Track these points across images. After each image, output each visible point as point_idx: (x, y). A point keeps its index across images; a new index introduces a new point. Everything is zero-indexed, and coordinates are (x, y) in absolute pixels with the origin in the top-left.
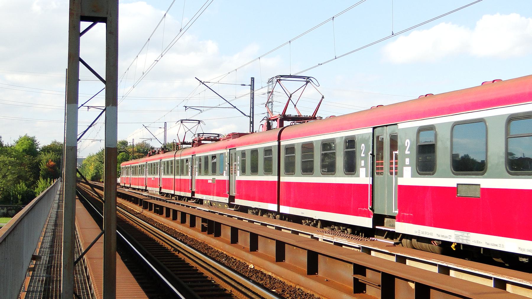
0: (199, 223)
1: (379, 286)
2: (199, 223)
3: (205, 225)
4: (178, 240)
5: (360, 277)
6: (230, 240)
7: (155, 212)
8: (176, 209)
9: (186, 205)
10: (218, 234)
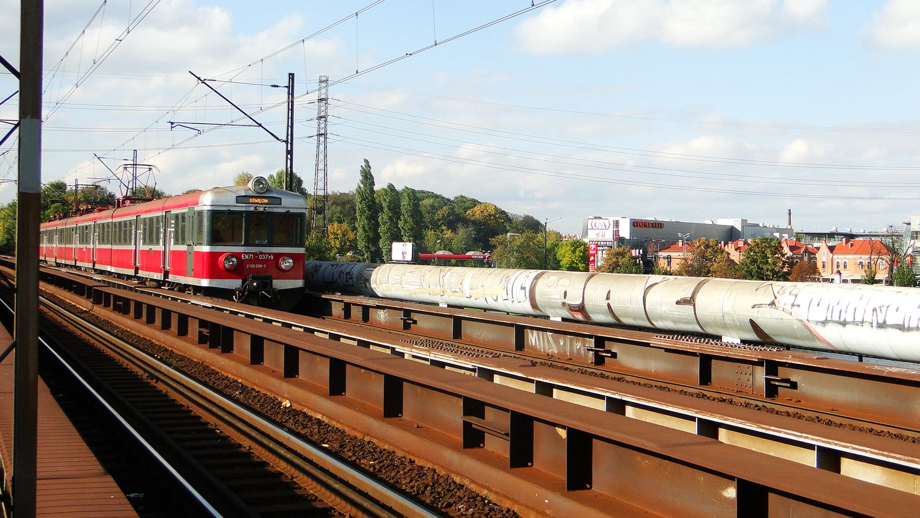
0: (194, 328)
1: (507, 435)
2: (194, 328)
3: (206, 332)
4: (156, 358)
5: (474, 420)
6: (327, 387)
7: (114, 309)
8: (153, 303)
9: (171, 297)
10: (227, 348)
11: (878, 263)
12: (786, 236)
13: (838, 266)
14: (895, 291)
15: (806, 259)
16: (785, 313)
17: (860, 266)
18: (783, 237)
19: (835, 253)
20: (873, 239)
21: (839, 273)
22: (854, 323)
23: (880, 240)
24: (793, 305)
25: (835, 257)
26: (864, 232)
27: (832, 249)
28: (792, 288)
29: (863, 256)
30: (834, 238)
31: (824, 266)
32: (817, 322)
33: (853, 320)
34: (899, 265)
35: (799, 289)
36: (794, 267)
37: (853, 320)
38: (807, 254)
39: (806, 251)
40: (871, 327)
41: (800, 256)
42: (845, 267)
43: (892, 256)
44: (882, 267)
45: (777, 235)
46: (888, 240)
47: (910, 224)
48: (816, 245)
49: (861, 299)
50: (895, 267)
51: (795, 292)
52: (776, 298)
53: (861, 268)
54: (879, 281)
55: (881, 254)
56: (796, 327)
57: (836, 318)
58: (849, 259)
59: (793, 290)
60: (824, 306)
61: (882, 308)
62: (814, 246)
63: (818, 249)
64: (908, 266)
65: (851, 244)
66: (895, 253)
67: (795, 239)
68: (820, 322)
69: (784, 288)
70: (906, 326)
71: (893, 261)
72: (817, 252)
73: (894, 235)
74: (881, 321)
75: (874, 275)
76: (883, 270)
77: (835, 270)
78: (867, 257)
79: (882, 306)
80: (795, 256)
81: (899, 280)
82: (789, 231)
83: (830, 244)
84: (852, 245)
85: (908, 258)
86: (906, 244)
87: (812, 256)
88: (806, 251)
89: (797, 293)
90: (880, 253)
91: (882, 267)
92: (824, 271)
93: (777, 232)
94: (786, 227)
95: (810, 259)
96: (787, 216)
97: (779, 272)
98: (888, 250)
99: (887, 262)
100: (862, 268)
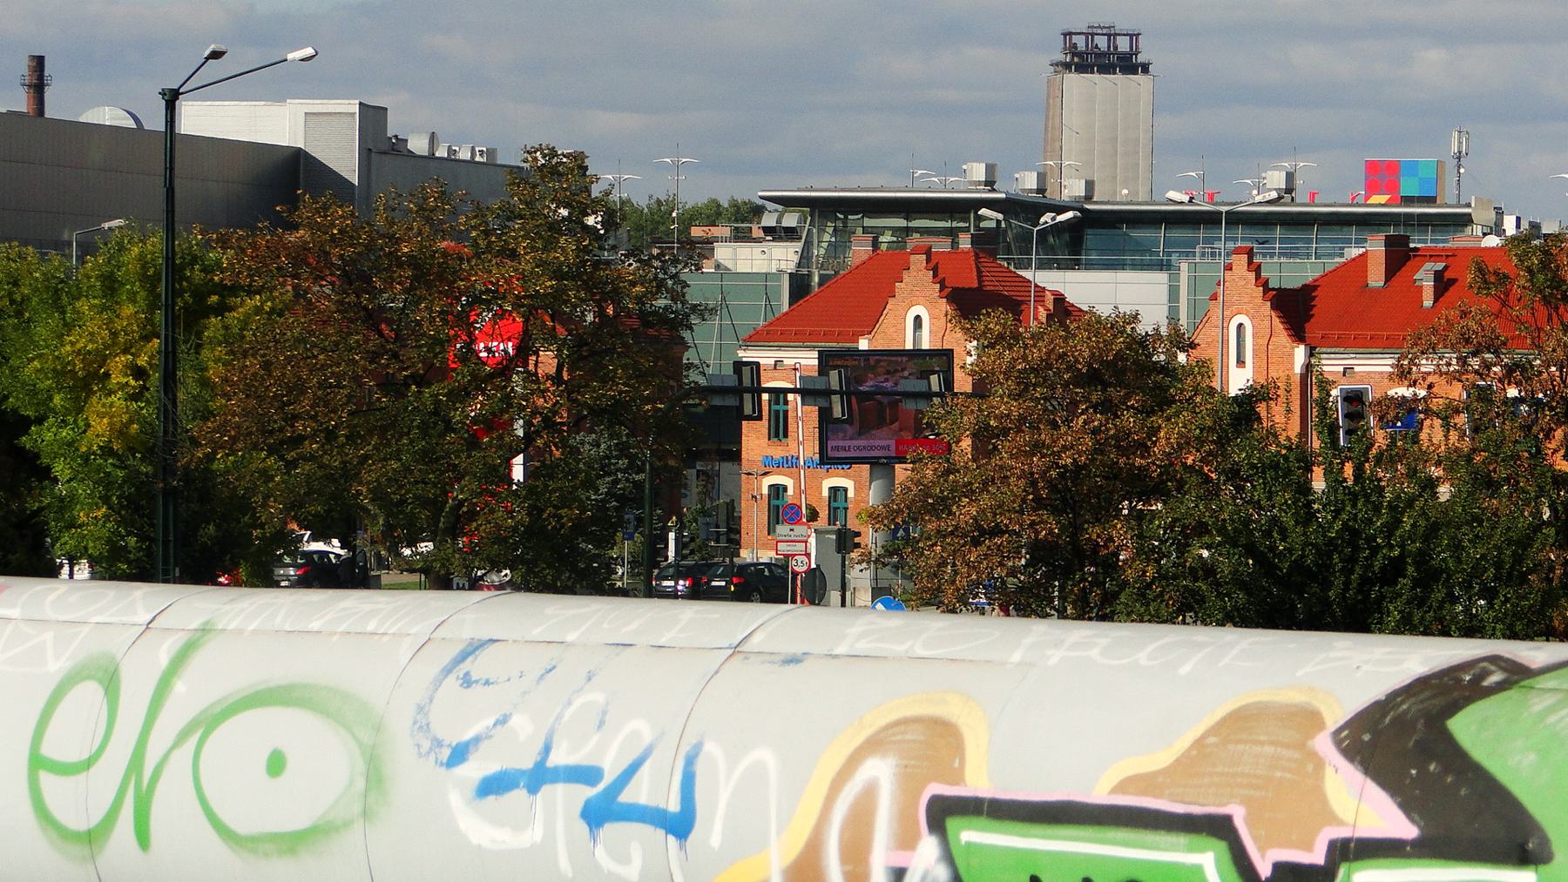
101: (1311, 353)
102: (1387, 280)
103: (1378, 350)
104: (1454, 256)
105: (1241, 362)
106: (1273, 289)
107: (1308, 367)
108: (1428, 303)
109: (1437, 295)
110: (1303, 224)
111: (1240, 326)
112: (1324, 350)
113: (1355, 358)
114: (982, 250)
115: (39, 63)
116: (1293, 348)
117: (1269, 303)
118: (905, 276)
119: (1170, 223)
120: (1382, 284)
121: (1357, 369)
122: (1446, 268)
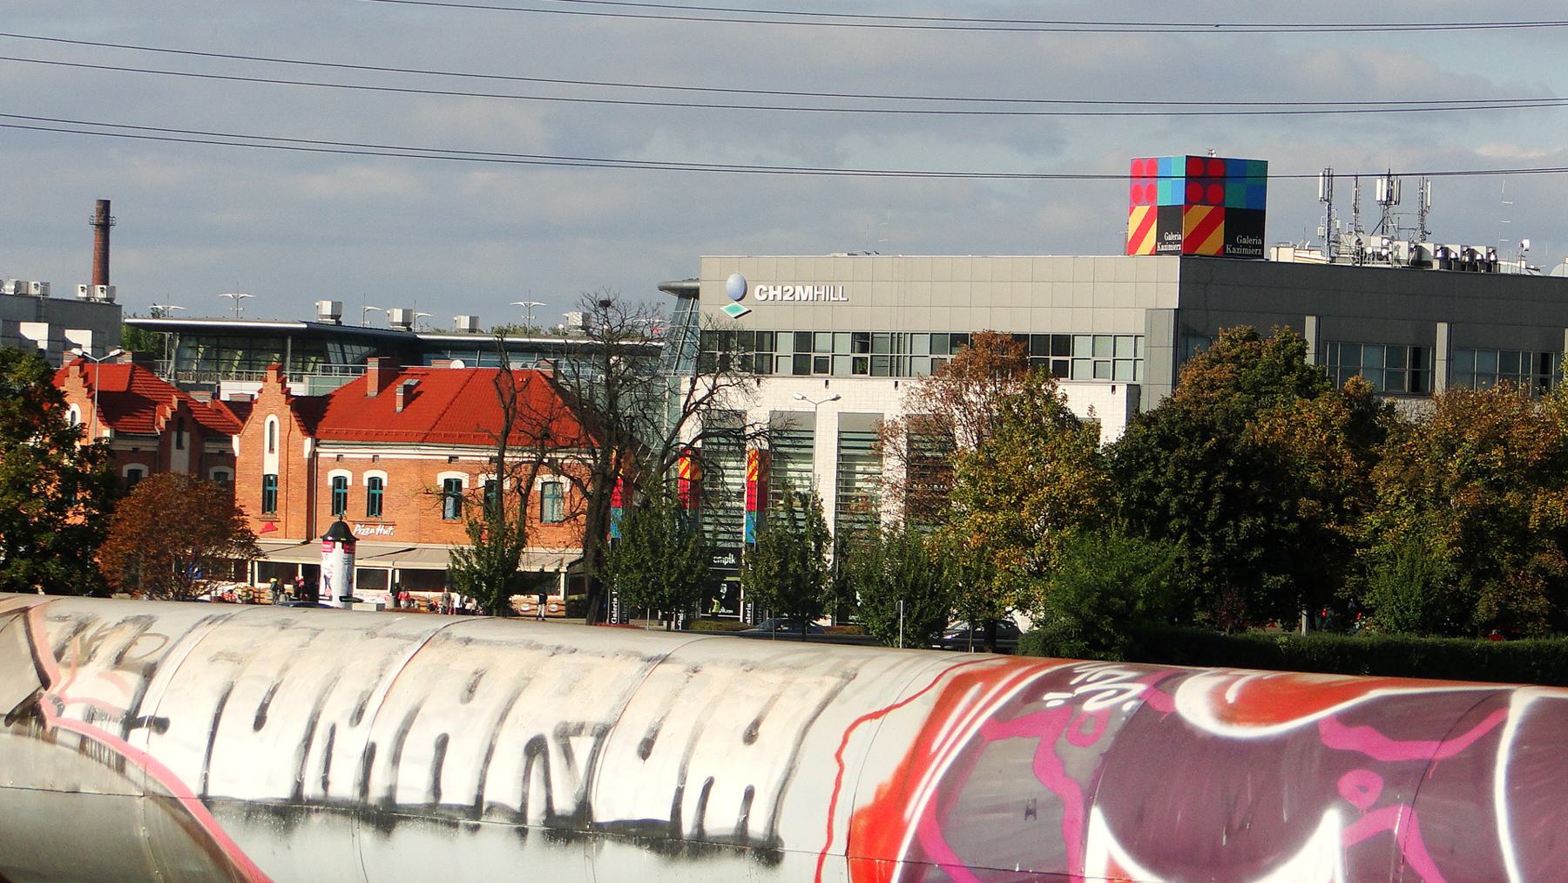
11: (537, 487)
12: (82, 339)
13: (339, 503)
14: (637, 654)
15: (180, 460)
16: (94, 763)
17: (450, 501)
18: (69, 345)
19: (328, 435)
20: (515, 365)
21: (343, 535)
22: (436, 814)
23: (549, 371)
24: (131, 721)
25: (326, 453)
26: (472, 330)
27: (309, 414)
28: (130, 631)
29: (466, 455)
30: (323, 354)
31: (269, 502)
32: (252, 810)
33: (431, 800)
34: (637, 499)
35: (167, 639)
36: (125, 505)
37: (431, 800)
38: (186, 436)
39: (184, 418)
40: (515, 839)
41: (149, 446)
42: (375, 504)
43: (606, 455)
44: (553, 511)
45: (36, 332)
46: (589, 370)
47: (693, 294)
48: (231, 389)
49: (471, 690)
50: (617, 513)
51: (143, 651)
52: (45, 682)
53: (450, 513)
54: (541, 583)
55: (549, 445)
56: (142, 832)
57: (344, 786)
58: (394, 467)
59: (133, 643)
60: (287, 724)
61: (574, 741)
62: (224, 396)
63: (243, 409)
64: (681, 508)
65: (408, 389)
66: (619, 441)
67: (127, 359)
68: (267, 807)
69: (89, 633)
70: (687, 828)
71: (604, 478)
72: (237, 430)
73: (619, 350)
74: (564, 803)
75: (517, 550)
76: (561, 523)
77: (325, 520)
78: (483, 456)
79: (571, 728)
80: (124, 446)
81: (637, 575)
82: (101, 316)
83: (299, 389)
84: (410, 395)
85: (683, 467)
86: (675, 392)
87: (211, 448)
88: (184, 418)
89: (150, 659)
90: (547, 436)
91: (553, 511)
92: (270, 528)
93: (38, 320)
94: (82, 295)
95: (200, 462)
96: (90, 236)
97: (43, 527)
98: (582, 421)
99: (576, 482)
100: (457, 512)
101: (316, 444)
102: (380, 391)
103: (336, 442)
104: (427, 374)
105: (271, 450)
106: (293, 396)
107: (314, 454)
108: (399, 408)
109: (406, 403)
110: (468, 350)
111: (272, 422)
112: (325, 441)
113: (343, 448)
114: (140, 364)
115: (105, 206)
116: (303, 439)
117: (289, 406)
118: (66, 382)
119: (485, 351)
120: (376, 393)
121: (345, 456)
122: (418, 383)
